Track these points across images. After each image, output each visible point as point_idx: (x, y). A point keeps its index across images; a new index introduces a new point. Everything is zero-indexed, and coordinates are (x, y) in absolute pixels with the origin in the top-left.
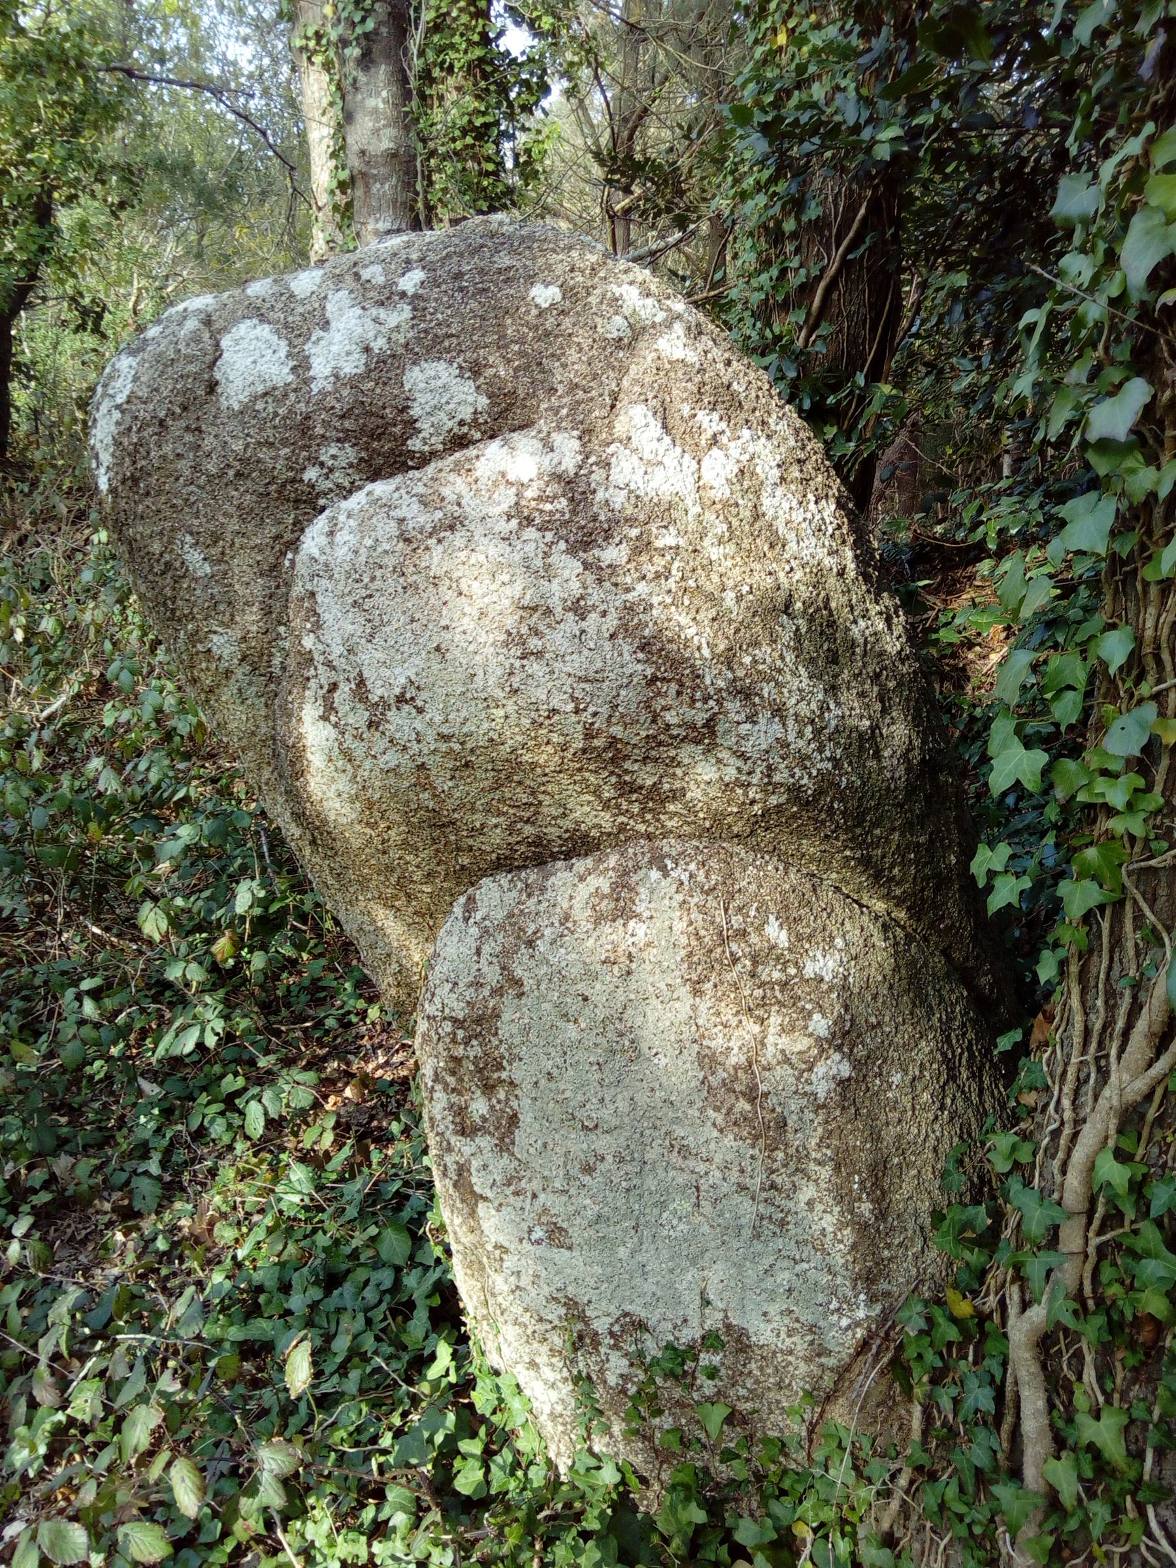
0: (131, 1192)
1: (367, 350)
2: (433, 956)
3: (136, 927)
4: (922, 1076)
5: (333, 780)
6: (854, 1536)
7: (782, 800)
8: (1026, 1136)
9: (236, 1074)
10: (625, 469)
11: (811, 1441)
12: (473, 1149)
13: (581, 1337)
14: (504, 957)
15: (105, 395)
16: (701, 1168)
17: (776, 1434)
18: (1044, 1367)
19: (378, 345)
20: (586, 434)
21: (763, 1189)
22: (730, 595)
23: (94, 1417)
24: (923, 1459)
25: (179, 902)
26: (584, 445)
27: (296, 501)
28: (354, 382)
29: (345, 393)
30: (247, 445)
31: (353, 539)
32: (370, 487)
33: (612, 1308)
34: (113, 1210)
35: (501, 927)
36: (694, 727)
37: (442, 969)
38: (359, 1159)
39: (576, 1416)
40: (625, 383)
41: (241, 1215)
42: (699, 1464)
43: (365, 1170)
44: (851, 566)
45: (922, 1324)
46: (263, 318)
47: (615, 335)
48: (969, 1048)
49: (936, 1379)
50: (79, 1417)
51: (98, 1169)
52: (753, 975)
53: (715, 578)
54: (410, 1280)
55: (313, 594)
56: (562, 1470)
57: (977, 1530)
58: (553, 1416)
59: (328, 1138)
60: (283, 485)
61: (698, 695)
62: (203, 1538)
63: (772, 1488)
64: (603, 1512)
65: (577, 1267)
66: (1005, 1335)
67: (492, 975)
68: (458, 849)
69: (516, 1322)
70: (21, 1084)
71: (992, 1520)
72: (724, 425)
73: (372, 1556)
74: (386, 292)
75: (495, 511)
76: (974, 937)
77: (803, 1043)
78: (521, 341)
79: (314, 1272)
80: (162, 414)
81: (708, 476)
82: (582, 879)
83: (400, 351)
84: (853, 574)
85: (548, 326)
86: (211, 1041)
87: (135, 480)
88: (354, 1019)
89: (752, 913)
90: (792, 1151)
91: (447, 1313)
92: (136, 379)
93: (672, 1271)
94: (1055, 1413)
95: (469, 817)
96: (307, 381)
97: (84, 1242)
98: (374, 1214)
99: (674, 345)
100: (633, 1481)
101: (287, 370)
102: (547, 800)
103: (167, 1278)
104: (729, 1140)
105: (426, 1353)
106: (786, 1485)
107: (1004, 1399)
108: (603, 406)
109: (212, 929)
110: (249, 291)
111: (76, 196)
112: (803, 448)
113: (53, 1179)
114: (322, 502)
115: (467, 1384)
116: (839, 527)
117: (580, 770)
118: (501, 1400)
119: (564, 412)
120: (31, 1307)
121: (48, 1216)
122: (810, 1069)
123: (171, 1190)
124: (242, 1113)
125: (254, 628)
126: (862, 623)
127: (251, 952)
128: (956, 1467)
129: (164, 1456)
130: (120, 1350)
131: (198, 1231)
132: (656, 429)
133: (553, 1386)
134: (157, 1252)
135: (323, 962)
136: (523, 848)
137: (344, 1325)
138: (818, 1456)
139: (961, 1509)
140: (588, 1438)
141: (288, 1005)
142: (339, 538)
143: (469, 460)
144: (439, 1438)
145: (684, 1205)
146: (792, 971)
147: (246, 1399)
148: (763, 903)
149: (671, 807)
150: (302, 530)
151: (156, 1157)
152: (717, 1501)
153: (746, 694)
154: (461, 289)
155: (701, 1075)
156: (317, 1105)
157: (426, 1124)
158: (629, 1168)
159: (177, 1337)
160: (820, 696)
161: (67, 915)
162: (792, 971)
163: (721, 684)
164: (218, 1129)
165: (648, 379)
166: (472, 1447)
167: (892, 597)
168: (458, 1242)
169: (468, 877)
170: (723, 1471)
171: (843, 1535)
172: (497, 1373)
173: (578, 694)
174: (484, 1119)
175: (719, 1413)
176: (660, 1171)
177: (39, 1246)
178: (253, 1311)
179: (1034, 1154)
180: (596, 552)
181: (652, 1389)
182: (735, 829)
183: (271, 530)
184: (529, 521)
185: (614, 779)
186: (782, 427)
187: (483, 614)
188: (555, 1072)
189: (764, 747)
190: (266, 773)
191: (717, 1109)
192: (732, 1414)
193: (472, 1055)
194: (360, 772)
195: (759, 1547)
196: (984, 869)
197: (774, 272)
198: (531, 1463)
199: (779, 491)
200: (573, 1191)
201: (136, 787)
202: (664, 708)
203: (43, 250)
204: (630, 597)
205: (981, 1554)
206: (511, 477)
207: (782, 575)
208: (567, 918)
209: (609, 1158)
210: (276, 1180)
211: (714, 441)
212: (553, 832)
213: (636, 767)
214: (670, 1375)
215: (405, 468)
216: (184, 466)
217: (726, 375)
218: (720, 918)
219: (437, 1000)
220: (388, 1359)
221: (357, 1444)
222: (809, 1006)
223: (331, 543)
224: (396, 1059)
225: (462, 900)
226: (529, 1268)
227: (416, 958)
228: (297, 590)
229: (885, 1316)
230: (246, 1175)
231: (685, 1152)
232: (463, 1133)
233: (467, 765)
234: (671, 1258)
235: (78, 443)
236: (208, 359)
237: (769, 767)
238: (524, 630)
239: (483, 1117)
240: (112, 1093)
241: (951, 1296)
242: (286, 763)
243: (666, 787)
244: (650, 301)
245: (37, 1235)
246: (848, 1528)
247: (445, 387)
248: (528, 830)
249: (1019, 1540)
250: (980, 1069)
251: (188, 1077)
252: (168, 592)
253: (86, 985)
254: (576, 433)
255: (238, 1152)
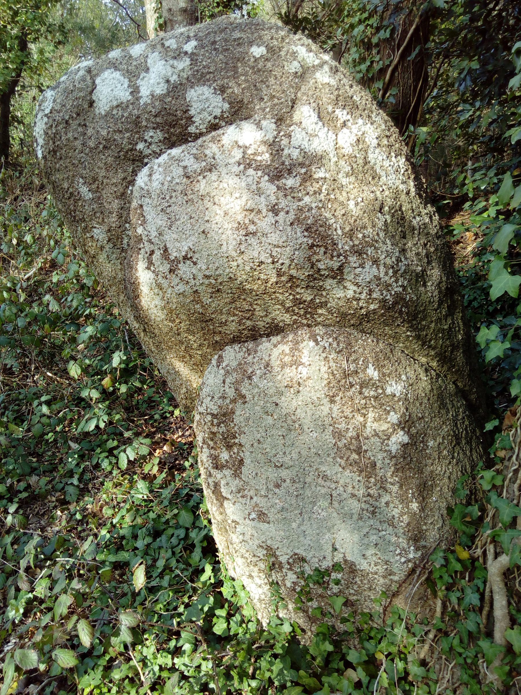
0: (65, 492)
1: (168, 81)
2: (200, 382)
3: (68, 373)
4: (443, 443)
5: (153, 299)
6: (405, 660)
7: (376, 307)
8: (498, 472)
9: (113, 440)
10: (299, 137)
11: (385, 615)
12: (222, 476)
13: (273, 564)
14: (237, 384)
15: (40, 110)
16: (333, 486)
17: (368, 611)
18: (506, 584)
19: (174, 78)
20: (280, 121)
21: (364, 496)
22: (352, 204)
23: (45, 596)
24: (442, 626)
25: (87, 361)
26: (278, 127)
27: (133, 160)
28: (161, 98)
29: (157, 103)
30: (109, 132)
31: (161, 178)
32: (169, 151)
33: (289, 551)
34: (57, 501)
35: (235, 370)
36: (333, 270)
37: (206, 390)
38: (169, 478)
39: (271, 601)
40: (299, 95)
41: (115, 503)
42: (330, 624)
43: (173, 483)
44: (413, 190)
45: (443, 562)
46: (116, 69)
47: (294, 70)
48: (466, 429)
49: (449, 588)
50: (39, 596)
51: (50, 482)
52: (361, 393)
53: (344, 194)
54: (193, 534)
55: (141, 206)
56: (265, 625)
57: (469, 661)
58: (260, 600)
59: (156, 469)
60: (127, 152)
61: (335, 254)
62: (95, 653)
63: (364, 635)
64: (284, 645)
65: (272, 532)
66: (486, 568)
67: (231, 393)
68: (214, 333)
69: (242, 557)
70: (14, 443)
71: (476, 656)
72: (349, 117)
73: (174, 664)
74: (178, 52)
75: (232, 161)
76: (469, 375)
77: (385, 427)
78: (246, 74)
79: (148, 530)
80: (67, 118)
81: (341, 143)
82: (275, 346)
83: (184, 81)
84: (413, 194)
85: (259, 66)
86: (102, 425)
87: (55, 152)
88: (168, 415)
89: (361, 363)
90: (378, 478)
91: (210, 549)
92: (54, 101)
93: (318, 534)
94: (511, 607)
95: (219, 316)
96: (138, 99)
97: (43, 515)
98: (176, 503)
99: (323, 77)
100: (298, 631)
101: (128, 94)
102: (258, 308)
103: (80, 532)
104: (347, 473)
105: (200, 568)
106: (372, 634)
107: (485, 601)
108: (287, 107)
109: (103, 374)
110: (110, 56)
111: (38, 38)
112: (389, 130)
113: (28, 487)
114: (146, 160)
115: (220, 583)
116: (407, 170)
117: (274, 292)
118: (235, 592)
119: (268, 110)
120: (18, 544)
121: (27, 503)
122: (388, 439)
123: (83, 491)
124: (117, 458)
125: (114, 225)
126: (418, 219)
127: (120, 384)
128: (460, 631)
129: (75, 618)
130: (58, 565)
131: (95, 511)
132: (314, 117)
133: (260, 586)
134: (76, 520)
135: (154, 389)
136: (246, 332)
137: (162, 555)
138: (389, 622)
139: (461, 650)
140: (277, 610)
141: (138, 409)
142: (154, 177)
143: (219, 136)
144: (206, 609)
145: (324, 503)
146: (380, 391)
147: (116, 588)
148: (366, 358)
149: (320, 311)
150: (136, 175)
151: (76, 476)
152: (338, 640)
153: (360, 253)
154: (215, 49)
155: (334, 441)
156: (151, 454)
157: (199, 464)
158: (297, 485)
159: (84, 559)
160: (397, 254)
161: (36, 368)
162: (380, 391)
163: (347, 248)
164: (105, 465)
165: (310, 93)
166: (222, 613)
167: (432, 207)
168: (215, 519)
169: (218, 346)
170: (341, 627)
171: (401, 660)
172: (233, 579)
173: (274, 254)
174: (227, 462)
175: (340, 601)
176: (313, 487)
177: (21, 517)
178: (120, 548)
179: (504, 481)
180: (284, 181)
181: (308, 589)
182: (352, 322)
183: (121, 175)
184: (250, 165)
185: (291, 297)
186: (378, 119)
187: (226, 214)
188: (262, 440)
189: (368, 280)
190: (122, 297)
191: (341, 458)
192: (347, 601)
193: (221, 431)
194: (166, 295)
195: (359, 664)
196: (484, 339)
197: (368, 63)
198: (249, 621)
199: (377, 151)
200: (270, 496)
201: (67, 309)
202: (318, 261)
203: (23, 63)
204: (301, 204)
205: (470, 672)
206: (241, 144)
207: (378, 193)
208: (268, 365)
209: (288, 481)
210: (131, 487)
211: (344, 124)
212: (261, 324)
213: (303, 291)
214: (317, 583)
215: (186, 141)
216: (78, 144)
217: (351, 92)
218: (345, 365)
219: (204, 405)
220: (182, 571)
221: (167, 610)
222: (388, 408)
223: (150, 180)
224: (187, 433)
225: (216, 357)
226: (249, 531)
227: (195, 386)
228: (134, 204)
229: (422, 558)
230: (117, 485)
231: (325, 478)
232: (217, 468)
233: (218, 291)
234: (318, 528)
235: (32, 153)
236: (89, 89)
237: (370, 290)
238: (247, 221)
239: (226, 460)
240: (57, 448)
241: (458, 548)
242: (130, 290)
243: (318, 301)
244: (311, 54)
245: (21, 512)
246: (402, 656)
247: (207, 99)
248: (249, 323)
249: (490, 666)
250: (471, 439)
251: (92, 442)
252: (72, 207)
253: (43, 399)
254: (273, 120)
255: (114, 475)
